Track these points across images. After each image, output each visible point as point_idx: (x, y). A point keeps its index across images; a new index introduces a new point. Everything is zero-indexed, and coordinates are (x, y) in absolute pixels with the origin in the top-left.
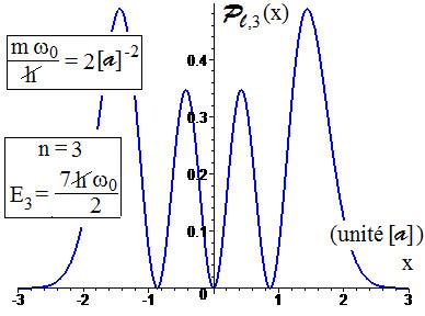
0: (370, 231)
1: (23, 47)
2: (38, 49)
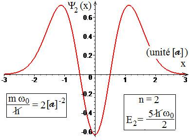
1: (14, 99)
2: (20, 100)
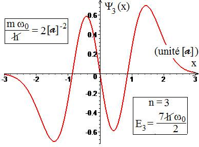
0: (173, 50)
1: (12, 24)
2: (19, 25)
